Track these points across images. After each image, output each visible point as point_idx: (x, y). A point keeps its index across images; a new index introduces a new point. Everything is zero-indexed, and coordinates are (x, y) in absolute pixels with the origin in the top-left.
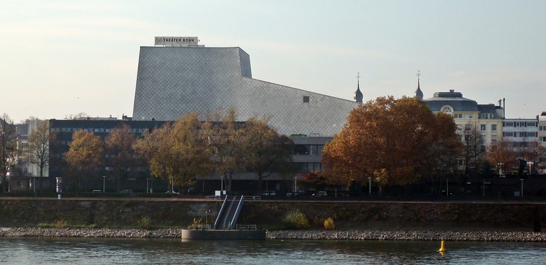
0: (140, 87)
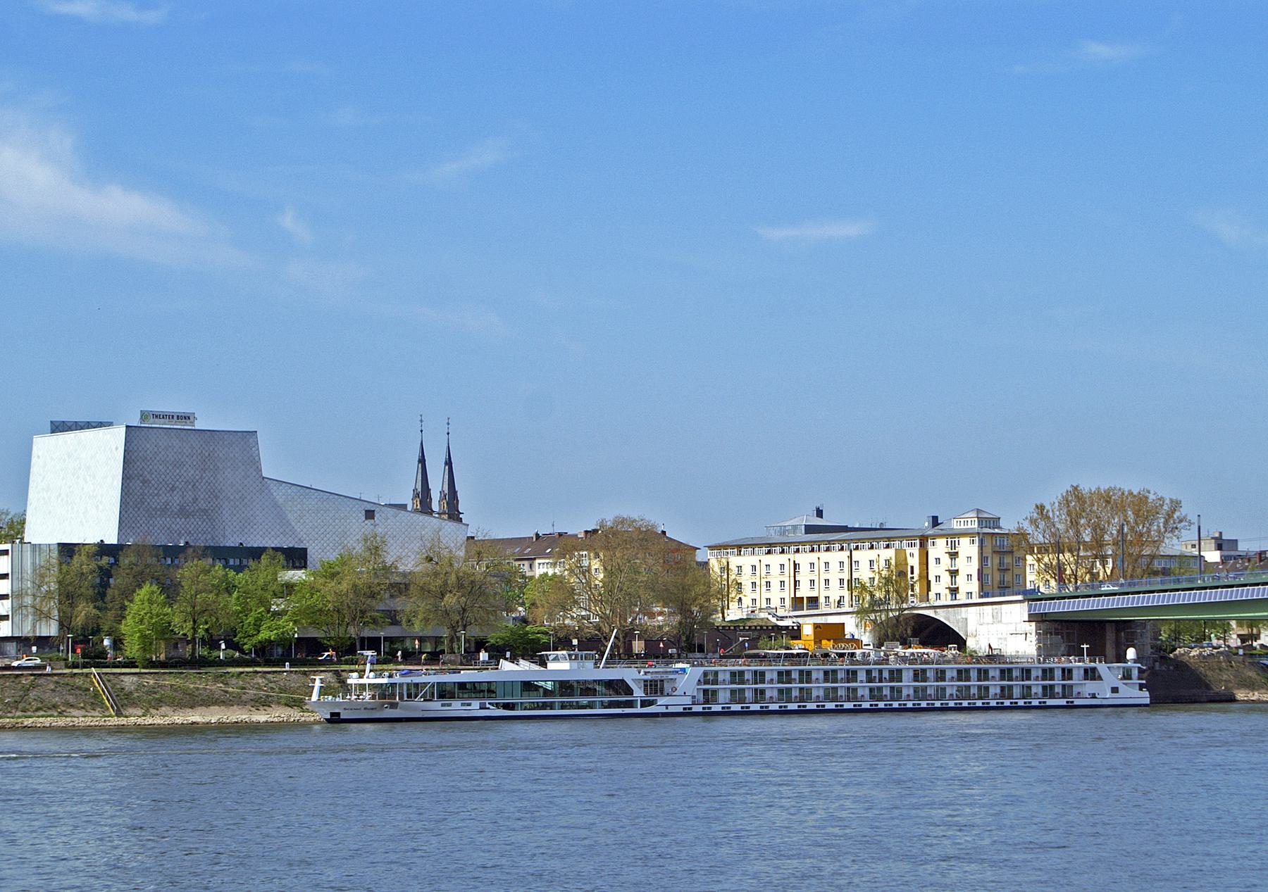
0: (126, 491)
